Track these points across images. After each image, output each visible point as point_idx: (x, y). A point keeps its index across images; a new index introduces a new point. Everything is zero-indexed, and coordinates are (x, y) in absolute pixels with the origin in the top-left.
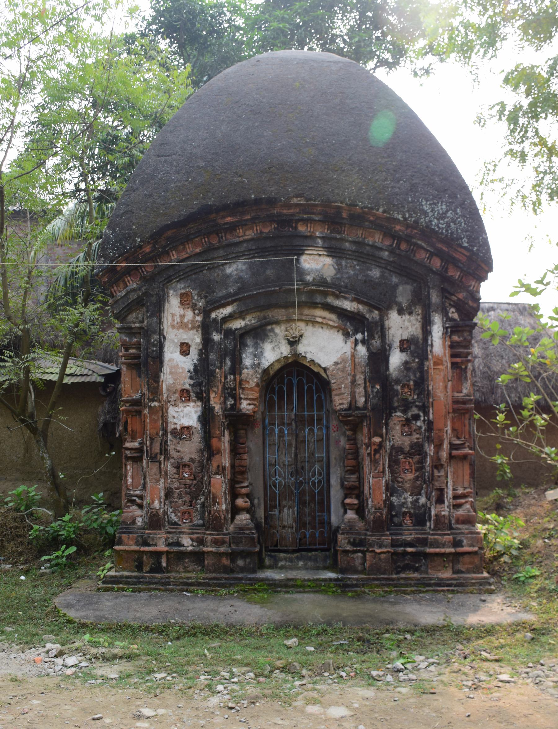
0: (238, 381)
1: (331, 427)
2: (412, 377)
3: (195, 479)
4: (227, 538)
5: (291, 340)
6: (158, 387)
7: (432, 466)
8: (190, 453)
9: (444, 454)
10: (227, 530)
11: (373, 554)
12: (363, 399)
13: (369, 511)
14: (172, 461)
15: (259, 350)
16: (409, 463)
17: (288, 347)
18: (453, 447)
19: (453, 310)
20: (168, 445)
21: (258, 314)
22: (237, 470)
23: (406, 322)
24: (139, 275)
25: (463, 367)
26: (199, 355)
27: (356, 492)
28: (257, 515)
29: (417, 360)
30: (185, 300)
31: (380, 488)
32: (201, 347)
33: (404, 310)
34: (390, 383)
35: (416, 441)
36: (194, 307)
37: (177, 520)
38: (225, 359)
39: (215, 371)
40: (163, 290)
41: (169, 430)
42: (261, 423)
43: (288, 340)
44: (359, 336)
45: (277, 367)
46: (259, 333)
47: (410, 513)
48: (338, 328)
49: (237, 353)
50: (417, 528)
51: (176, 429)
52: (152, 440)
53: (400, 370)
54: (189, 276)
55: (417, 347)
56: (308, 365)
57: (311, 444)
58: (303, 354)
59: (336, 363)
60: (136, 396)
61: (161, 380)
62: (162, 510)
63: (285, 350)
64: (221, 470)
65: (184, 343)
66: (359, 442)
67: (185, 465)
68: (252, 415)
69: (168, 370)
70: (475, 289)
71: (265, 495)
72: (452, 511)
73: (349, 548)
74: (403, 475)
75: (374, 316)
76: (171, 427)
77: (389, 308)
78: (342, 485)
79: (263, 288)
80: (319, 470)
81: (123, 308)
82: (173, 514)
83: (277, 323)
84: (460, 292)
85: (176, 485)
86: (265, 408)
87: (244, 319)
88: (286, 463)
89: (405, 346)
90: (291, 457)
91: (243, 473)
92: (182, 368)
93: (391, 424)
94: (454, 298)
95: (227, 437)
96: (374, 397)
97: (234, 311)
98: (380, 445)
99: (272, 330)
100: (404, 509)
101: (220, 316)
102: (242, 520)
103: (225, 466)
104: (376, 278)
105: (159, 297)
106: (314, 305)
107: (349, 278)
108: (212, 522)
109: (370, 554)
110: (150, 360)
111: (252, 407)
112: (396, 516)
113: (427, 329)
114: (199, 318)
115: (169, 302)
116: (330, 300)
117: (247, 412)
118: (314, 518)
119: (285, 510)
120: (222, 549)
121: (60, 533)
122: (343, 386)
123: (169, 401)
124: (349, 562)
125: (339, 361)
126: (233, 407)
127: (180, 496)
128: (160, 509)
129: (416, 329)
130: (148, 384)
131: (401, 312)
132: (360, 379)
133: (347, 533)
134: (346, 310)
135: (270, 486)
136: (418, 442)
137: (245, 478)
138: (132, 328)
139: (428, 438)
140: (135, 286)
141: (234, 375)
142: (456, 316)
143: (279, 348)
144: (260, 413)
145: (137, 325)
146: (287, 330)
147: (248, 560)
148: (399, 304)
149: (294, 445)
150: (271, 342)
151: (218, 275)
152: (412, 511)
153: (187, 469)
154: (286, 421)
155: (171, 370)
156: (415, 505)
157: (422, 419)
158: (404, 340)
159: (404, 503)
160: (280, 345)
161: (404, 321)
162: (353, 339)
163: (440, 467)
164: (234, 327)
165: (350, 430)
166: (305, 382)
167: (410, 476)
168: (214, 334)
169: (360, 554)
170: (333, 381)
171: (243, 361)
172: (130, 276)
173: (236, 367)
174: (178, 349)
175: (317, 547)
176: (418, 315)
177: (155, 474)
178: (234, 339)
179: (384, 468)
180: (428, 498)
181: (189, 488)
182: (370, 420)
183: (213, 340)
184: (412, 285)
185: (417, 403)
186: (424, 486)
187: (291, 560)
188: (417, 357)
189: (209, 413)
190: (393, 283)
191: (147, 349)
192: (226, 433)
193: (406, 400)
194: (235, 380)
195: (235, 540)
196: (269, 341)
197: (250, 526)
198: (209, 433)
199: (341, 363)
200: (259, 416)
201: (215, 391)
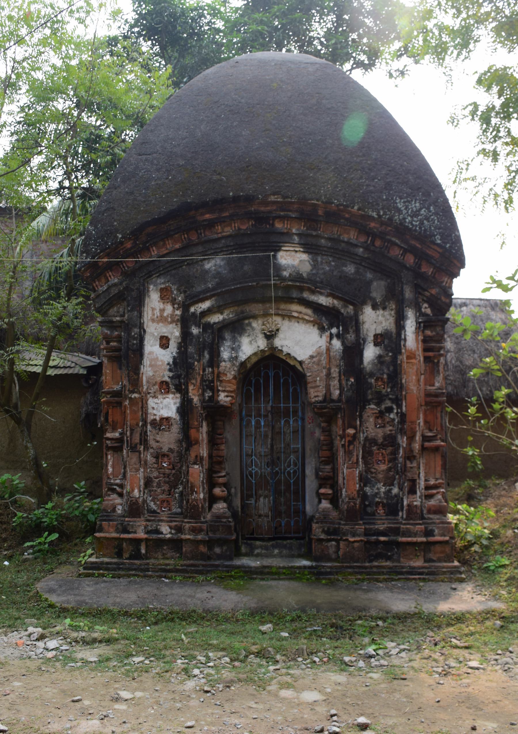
1: (307, 419)
2: (386, 371)
3: (173, 468)
5: (268, 333)
6: (138, 379)
8: (169, 444)
9: (417, 446)
11: (346, 543)
12: (337, 392)
13: (343, 501)
14: (151, 451)
15: (237, 344)
16: (382, 454)
18: (425, 438)
20: (147, 436)
21: (236, 308)
22: (214, 460)
25: (436, 361)
27: (330, 482)
29: (390, 354)
30: (165, 295)
32: (180, 340)
35: (389, 432)
36: (173, 302)
37: (156, 508)
38: (203, 352)
39: (194, 363)
40: (144, 285)
41: (149, 420)
43: (265, 334)
44: (334, 331)
45: (254, 360)
47: (382, 503)
48: (314, 323)
49: (215, 346)
50: (389, 517)
51: (155, 420)
52: (132, 430)
53: (373, 364)
54: (168, 271)
55: (390, 341)
56: (284, 358)
57: (287, 435)
59: (312, 357)
60: (117, 388)
61: (141, 372)
63: (262, 343)
64: (199, 460)
65: (164, 336)
67: (164, 455)
69: (148, 363)
72: (424, 501)
73: (323, 536)
74: (376, 466)
75: (349, 311)
76: (150, 418)
77: (364, 303)
78: (317, 476)
79: (240, 283)
80: (294, 460)
81: (105, 303)
82: (152, 503)
83: (255, 317)
84: (433, 288)
87: (222, 313)
88: (263, 454)
89: (378, 340)
90: (267, 448)
91: (220, 463)
92: (162, 361)
93: (365, 416)
97: (213, 306)
98: (354, 437)
99: (250, 324)
101: (199, 311)
102: (219, 509)
103: (203, 457)
104: (351, 274)
106: (290, 300)
107: (324, 273)
110: (130, 353)
111: (229, 399)
112: (369, 505)
113: (400, 324)
114: (178, 312)
115: (149, 296)
116: (306, 295)
117: (225, 404)
119: (262, 499)
120: (199, 537)
122: (318, 379)
123: (149, 393)
125: (315, 355)
126: (211, 398)
127: (159, 485)
128: (139, 497)
130: (128, 377)
131: (375, 307)
132: (335, 372)
133: (322, 522)
134: (321, 305)
135: (247, 476)
136: (391, 434)
140: (116, 280)
141: (212, 368)
142: (429, 311)
143: (256, 342)
146: (264, 325)
147: (225, 548)
148: (373, 300)
149: (270, 436)
150: (249, 336)
152: (385, 501)
153: (166, 459)
154: (262, 412)
155: (151, 362)
156: (388, 495)
157: (395, 411)
159: (377, 494)
160: (257, 339)
161: (378, 316)
162: (328, 334)
164: (212, 322)
166: (281, 374)
167: (383, 467)
168: (193, 328)
170: (308, 374)
171: (221, 354)
172: (111, 271)
173: (215, 360)
175: (292, 535)
177: (135, 464)
178: (213, 333)
179: (358, 459)
180: (401, 489)
182: (344, 413)
185: (391, 396)
186: (397, 477)
190: (368, 279)
191: (128, 343)
192: (204, 424)
193: (379, 393)
194: (213, 372)
195: (213, 527)
197: (227, 515)
198: (188, 423)
199: (316, 356)
201: (193, 384)
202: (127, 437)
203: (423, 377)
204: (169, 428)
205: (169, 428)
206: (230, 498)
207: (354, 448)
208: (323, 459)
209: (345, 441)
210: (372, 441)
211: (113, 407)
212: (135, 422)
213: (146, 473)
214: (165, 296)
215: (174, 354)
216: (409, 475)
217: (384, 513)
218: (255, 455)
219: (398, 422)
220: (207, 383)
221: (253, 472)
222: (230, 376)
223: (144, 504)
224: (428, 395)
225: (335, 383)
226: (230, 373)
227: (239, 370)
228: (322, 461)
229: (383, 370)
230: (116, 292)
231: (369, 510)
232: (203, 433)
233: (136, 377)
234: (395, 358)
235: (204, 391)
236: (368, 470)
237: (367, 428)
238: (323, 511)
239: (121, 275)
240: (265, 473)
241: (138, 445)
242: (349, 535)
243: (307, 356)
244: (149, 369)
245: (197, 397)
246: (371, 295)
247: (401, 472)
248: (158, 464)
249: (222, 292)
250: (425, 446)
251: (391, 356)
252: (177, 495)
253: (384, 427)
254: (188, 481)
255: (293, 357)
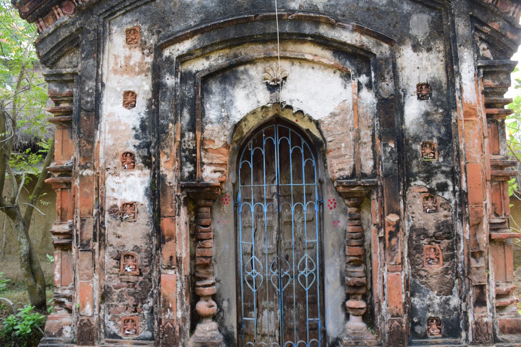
0: (199, 139)
1: (326, 203)
2: (435, 133)
3: (141, 274)
6: (92, 150)
7: (468, 253)
8: (135, 239)
9: (483, 237)
12: (371, 163)
13: (383, 319)
14: (110, 249)
15: (228, 99)
16: (435, 249)
17: (268, 93)
18: (494, 227)
19: (484, 46)
20: (105, 228)
21: (227, 51)
22: (198, 262)
23: (424, 60)
24: (73, 7)
25: (500, 121)
26: (148, 107)
27: (363, 291)
28: (227, 323)
29: (441, 111)
30: (132, 37)
31: (398, 287)
32: (150, 96)
33: (420, 45)
34: (407, 141)
35: (443, 219)
36: (143, 46)
37: (116, 331)
38: (182, 111)
39: (167, 126)
40: (104, 26)
41: (107, 207)
42: (231, 198)
43: (267, 84)
44: (363, 79)
45: (253, 123)
46: (227, 74)
47: (437, 319)
48: (335, 68)
49: (198, 102)
50: (448, 340)
51: (116, 206)
52: (83, 220)
53: (419, 124)
54: (137, 7)
55: (441, 94)
56: (293, 119)
58: (288, 103)
59: (333, 115)
60: (66, 163)
61: (97, 140)
62: (95, 318)
63: (264, 97)
64: (175, 262)
66: (365, 222)
67: (127, 256)
68: (218, 187)
69: (108, 128)
70: (515, 16)
71: (238, 294)
72: (495, 316)
74: (427, 267)
75: (383, 51)
76: (109, 204)
77: (401, 42)
78: (343, 282)
79: (233, 16)
80: (309, 259)
81: (52, 49)
82: (112, 323)
83: (252, 62)
84: (495, 21)
85: (116, 282)
86: (237, 180)
87: (207, 58)
88: (266, 252)
89: (424, 91)
90: (272, 243)
91: (206, 266)
92: (125, 124)
93: (410, 196)
94: (486, 29)
95: (183, 217)
96: (387, 159)
97: (195, 47)
98: (398, 226)
99: (246, 72)
100: (429, 315)
101: (176, 54)
102: (205, 332)
103: (181, 258)
104: (383, 5)
105: (98, 34)
106: (301, 38)
108: (163, 335)
110: (83, 114)
111: (218, 174)
112: (418, 323)
113: (453, 70)
114: (149, 60)
115: (111, 40)
116: (324, 30)
117: (212, 182)
119: (265, 313)
121: (16, 328)
122: (343, 145)
123: (108, 169)
125: (337, 112)
126: (192, 175)
127: (121, 298)
128: (93, 316)
129: (438, 69)
130: (80, 146)
131: (416, 48)
132: (366, 135)
134: (345, 44)
135: (244, 282)
136: (446, 221)
137: (209, 274)
138: (63, 75)
139: (461, 215)
140: (66, 18)
141: (194, 132)
142: (488, 54)
144: (230, 185)
145: (69, 70)
146: (265, 72)
148: (414, 38)
150: (245, 87)
152: (441, 317)
153: (130, 261)
154: (265, 196)
155: (111, 127)
156: (444, 308)
157: (451, 189)
158: (422, 85)
159: (429, 306)
160: (256, 91)
161: (421, 59)
162: (355, 82)
163: (478, 255)
164: (194, 70)
165: (353, 206)
166: (290, 143)
167: (437, 268)
170: (328, 139)
172: (61, 7)
173: (196, 123)
174: (121, 100)
176: (439, 52)
177: (87, 268)
178: (195, 84)
179: (402, 258)
180: (463, 298)
181: (133, 286)
182: (382, 192)
183: (165, 85)
184: (429, 14)
185: (444, 168)
186: (457, 281)
188: (441, 106)
189: (159, 183)
190: (405, 12)
191: (80, 101)
192: (183, 211)
193: (427, 164)
194: (195, 139)
196: (242, 86)
198: (159, 210)
199: (339, 114)
200: (228, 189)
201: (166, 154)
202: (77, 231)
203: (487, 141)
204: (134, 217)
205: (134, 217)
206: (221, 314)
207: (397, 241)
208: (352, 258)
210: (423, 232)
211: (62, 189)
212: (87, 210)
213: (102, 281)
214: (133, 39)
215: (143, 115)
216: (475, 279)
217: (440, 333)
219: (456, 204)
221: (254, 277)
222: (219, 143)
223: (100, 325)
224: (495, 166)
225: (367, 151)
227: (232, 136)
228: (350, 262)
229: (431, 133)
230: (67, 35)
231: (418, 329)
232: (180, 223)
233: (89, 147)
234: (447, 116)
235: (182, 165)
236: (416, 274)
237: (413, 213)
238: (354, 333)
239: (74, 13)
240: (269, 278)
241: (91, 242)
243: (327, 114)
244: (108, 136)
245: (172, 173)
246: (410, 32)
247: (463, 274)
248: (119, 268)
249: (207, 27)
250: (493, 238)
251: (441, 113)
253: (436, 211)
254: (160, 293)
255: (307, 115)
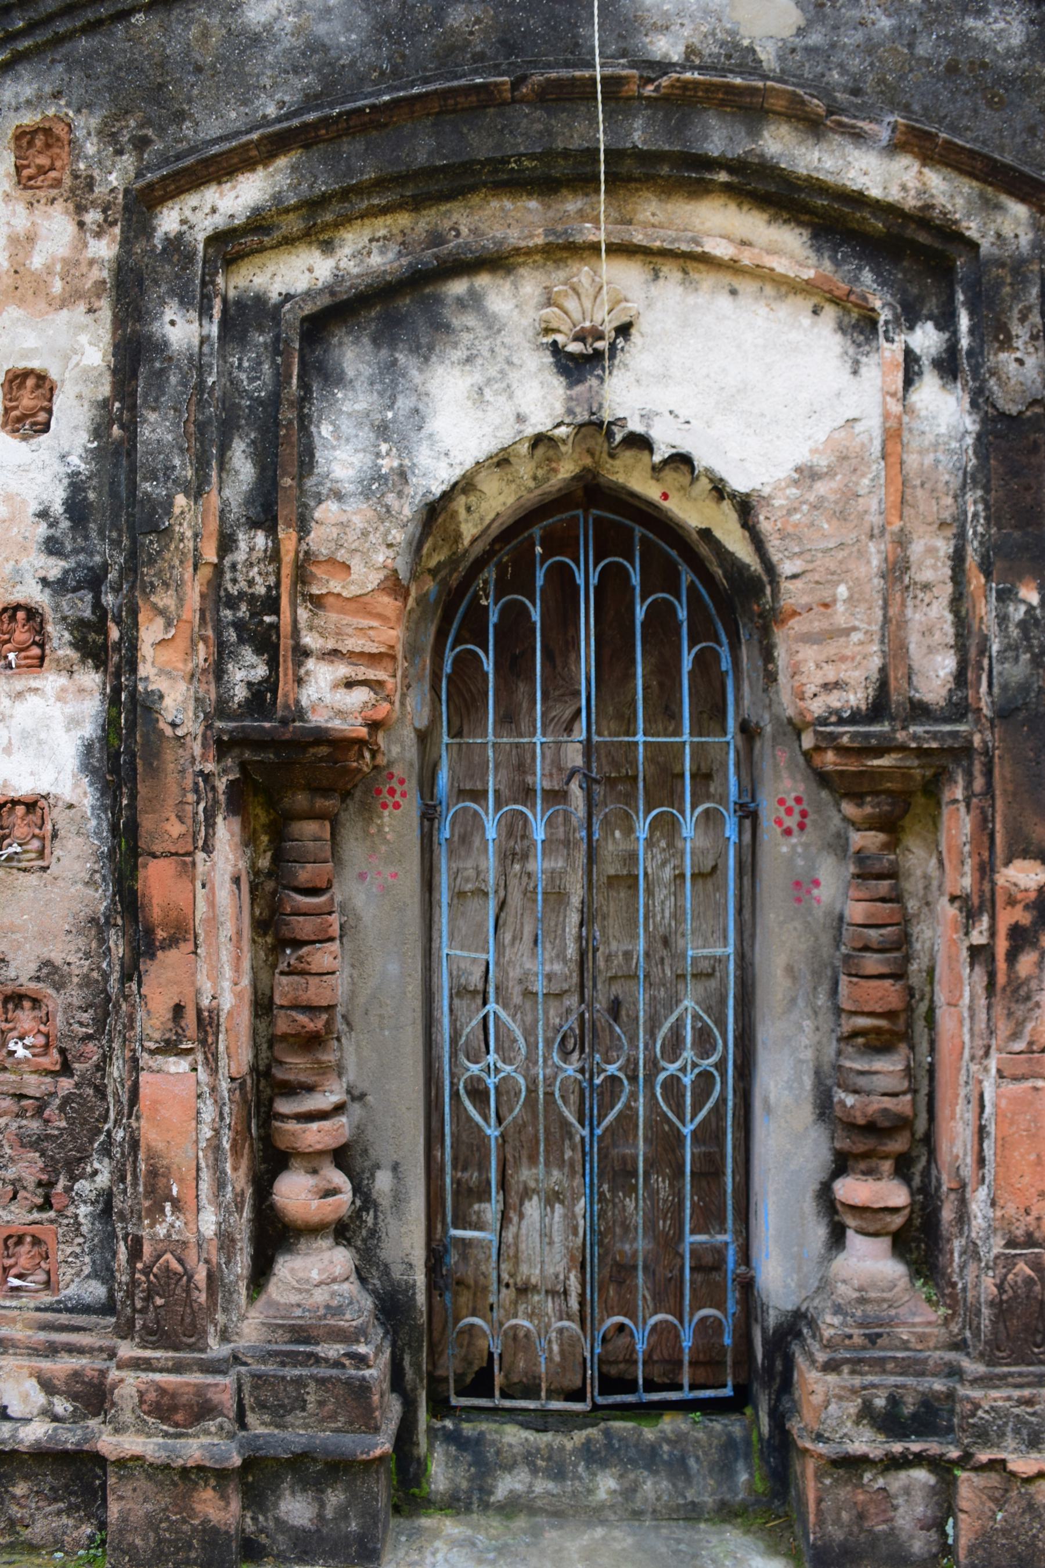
0: (288, 558)
1: (769, 810)
3: (66, 1069)
4: (222, 1388)
5: (575, 347)
8: (42, 936)
10: (224, 1336)
11: (993, 1479)
12: (946, 664)
13: (972, 1251)
15: (404, 403)
17: (557, 384)
21: (404, 219)
22: (282, 1026)
27: (898, 1145)
32: (105, 390)
36: (80, 195)
38: (224, 447)
42: (412, 786)
43: (556, 349)
44: (926, 339)
45: (498, 500)
46: (402, 309)
48: (818, 295)
49: (287, 414)
54: (59, 40)
56: (651, 490)
57: (660, 894)
58: (635, 426)
59: (807, 475)
63: (540, 400)
64: (193, 1030)
65: (27, 373)
68: (361, 742)
71: (432, 1138)
73: (864, 1442)
75: (1008, 230)
78: (824, 1107)
79: (426, 81)
83: (498, 262)
87: (328, 247)
88: (539, 986)
90: (561, 956)
91: (312, 1042)
95: (226, 854)
96: (1010, 649)
97: (277, 198)
99: (474, 302)
101: (205, 226)
102: (304, 1287)
103: (214, 1013)
104: (1009, 53)
106: (689, 174)
107: (869, 48)
109: (979, 1480)
111: (361, 695)
114: (105, 248)
116: (780, 145)
117: (337, 724)
118: (671, 1242)
119: (532, 1208)
120: (195, 1448)
122: (842, 591)
124: (861, 1516)
125: (822, 462)
126: (262, 695)
132: (931, 557)
133: (856, 1365)
134: (858, 199)
135: (455, 1095)
137: (323, 1069)
141: (271, 531)
143: (508, 391)
144: (409, 736)
146: (549, 302)
147: (335, 1498)
149: (575, 901)
150: (469, 360)
151: (205, 35)
153: (26, 1019)
154: (540, 781)
160: (514, 375)
162: (892, 351)
164: (275, 291)
166: (636, 580)
168: (169, 314)
169: (921, 1475)
171: (321, 456)
173: (280, 495)
175: (686, 1394)
178: (277, 347)
182: (988, 773)
183: (162, 346)
187: (558, 1472)
189: (132, 725)
194: (274, 556)
195: (269, 1394)
197: (349, 1321)
199: (830, 473)
200: (399, 750)
201: (162, 612)
204: (41, 854)
205: (41, 854)
209: (993, 933)
214: (42, 171)
215: (74, 460)
218: (503, 999)
220: (243, 609)
221: (491, 1082)
222: (365, 576)
225: (931, 617)
226: (366, 555)
235: (223, 654)
238: (862, 1301)
242: (1010, 1442)
243: (784, 471)
245: (182, 686)
252: (83, 1210)
255: (709, 472)
